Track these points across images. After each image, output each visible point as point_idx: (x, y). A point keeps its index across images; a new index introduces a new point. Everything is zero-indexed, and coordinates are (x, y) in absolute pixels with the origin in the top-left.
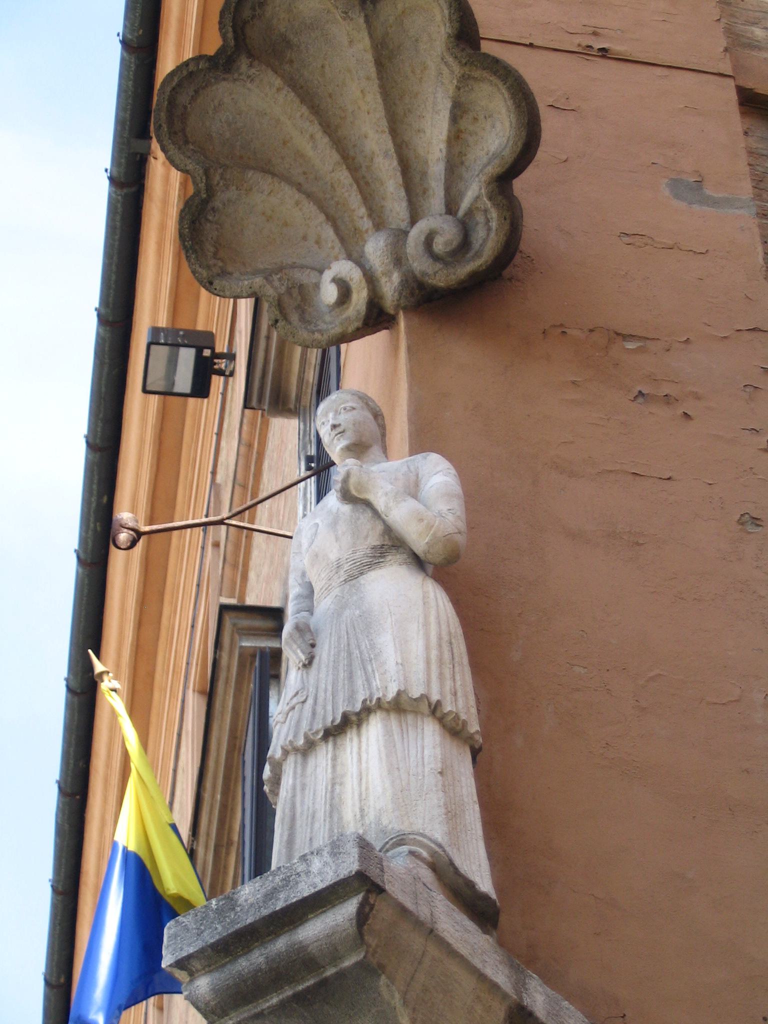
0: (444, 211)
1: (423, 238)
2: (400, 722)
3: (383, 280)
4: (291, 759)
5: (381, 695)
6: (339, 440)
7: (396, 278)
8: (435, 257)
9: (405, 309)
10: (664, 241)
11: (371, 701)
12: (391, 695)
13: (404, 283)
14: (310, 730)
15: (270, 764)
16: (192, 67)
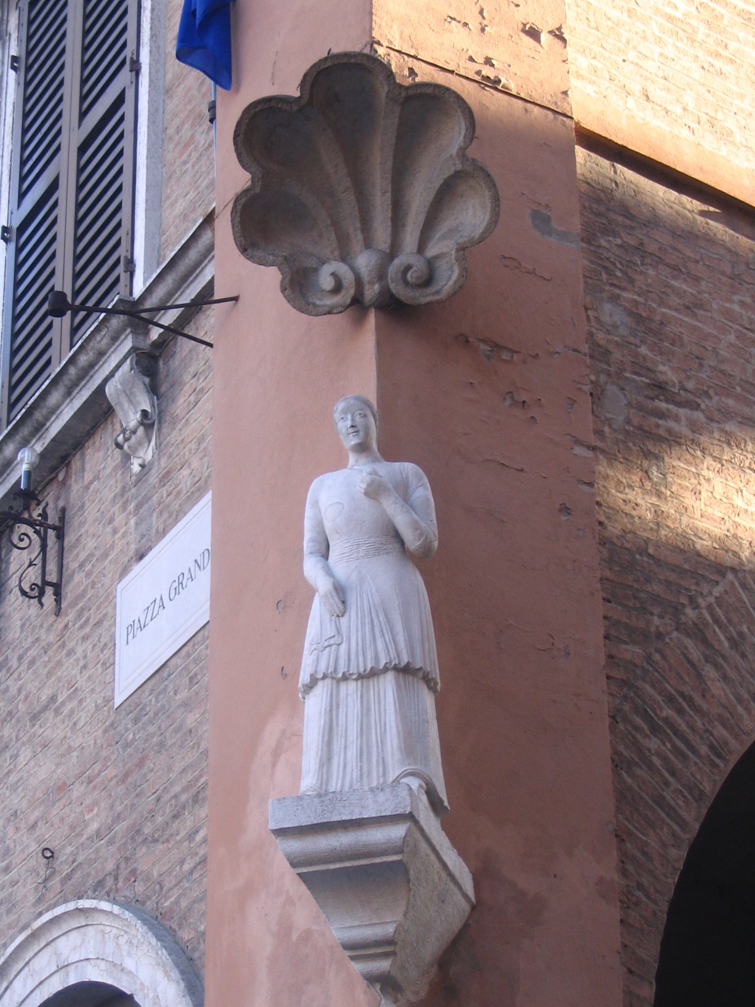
0: (415, 251)
1: (402, 268)
2: (405, 681)
3: (367, 287)
4: (328, 681)
5: (397, 662)
6: (354, 436)
7: (377, 287)
8: (406, 282)
9: (376, 308)
10: (528, 266)
11: (390, 665)
12: (403, 664)
13: (381, 293)
14: (348, 671)
15: (446, 808)
16: (273, 104)
